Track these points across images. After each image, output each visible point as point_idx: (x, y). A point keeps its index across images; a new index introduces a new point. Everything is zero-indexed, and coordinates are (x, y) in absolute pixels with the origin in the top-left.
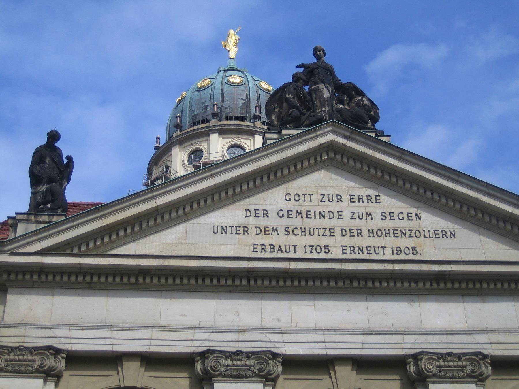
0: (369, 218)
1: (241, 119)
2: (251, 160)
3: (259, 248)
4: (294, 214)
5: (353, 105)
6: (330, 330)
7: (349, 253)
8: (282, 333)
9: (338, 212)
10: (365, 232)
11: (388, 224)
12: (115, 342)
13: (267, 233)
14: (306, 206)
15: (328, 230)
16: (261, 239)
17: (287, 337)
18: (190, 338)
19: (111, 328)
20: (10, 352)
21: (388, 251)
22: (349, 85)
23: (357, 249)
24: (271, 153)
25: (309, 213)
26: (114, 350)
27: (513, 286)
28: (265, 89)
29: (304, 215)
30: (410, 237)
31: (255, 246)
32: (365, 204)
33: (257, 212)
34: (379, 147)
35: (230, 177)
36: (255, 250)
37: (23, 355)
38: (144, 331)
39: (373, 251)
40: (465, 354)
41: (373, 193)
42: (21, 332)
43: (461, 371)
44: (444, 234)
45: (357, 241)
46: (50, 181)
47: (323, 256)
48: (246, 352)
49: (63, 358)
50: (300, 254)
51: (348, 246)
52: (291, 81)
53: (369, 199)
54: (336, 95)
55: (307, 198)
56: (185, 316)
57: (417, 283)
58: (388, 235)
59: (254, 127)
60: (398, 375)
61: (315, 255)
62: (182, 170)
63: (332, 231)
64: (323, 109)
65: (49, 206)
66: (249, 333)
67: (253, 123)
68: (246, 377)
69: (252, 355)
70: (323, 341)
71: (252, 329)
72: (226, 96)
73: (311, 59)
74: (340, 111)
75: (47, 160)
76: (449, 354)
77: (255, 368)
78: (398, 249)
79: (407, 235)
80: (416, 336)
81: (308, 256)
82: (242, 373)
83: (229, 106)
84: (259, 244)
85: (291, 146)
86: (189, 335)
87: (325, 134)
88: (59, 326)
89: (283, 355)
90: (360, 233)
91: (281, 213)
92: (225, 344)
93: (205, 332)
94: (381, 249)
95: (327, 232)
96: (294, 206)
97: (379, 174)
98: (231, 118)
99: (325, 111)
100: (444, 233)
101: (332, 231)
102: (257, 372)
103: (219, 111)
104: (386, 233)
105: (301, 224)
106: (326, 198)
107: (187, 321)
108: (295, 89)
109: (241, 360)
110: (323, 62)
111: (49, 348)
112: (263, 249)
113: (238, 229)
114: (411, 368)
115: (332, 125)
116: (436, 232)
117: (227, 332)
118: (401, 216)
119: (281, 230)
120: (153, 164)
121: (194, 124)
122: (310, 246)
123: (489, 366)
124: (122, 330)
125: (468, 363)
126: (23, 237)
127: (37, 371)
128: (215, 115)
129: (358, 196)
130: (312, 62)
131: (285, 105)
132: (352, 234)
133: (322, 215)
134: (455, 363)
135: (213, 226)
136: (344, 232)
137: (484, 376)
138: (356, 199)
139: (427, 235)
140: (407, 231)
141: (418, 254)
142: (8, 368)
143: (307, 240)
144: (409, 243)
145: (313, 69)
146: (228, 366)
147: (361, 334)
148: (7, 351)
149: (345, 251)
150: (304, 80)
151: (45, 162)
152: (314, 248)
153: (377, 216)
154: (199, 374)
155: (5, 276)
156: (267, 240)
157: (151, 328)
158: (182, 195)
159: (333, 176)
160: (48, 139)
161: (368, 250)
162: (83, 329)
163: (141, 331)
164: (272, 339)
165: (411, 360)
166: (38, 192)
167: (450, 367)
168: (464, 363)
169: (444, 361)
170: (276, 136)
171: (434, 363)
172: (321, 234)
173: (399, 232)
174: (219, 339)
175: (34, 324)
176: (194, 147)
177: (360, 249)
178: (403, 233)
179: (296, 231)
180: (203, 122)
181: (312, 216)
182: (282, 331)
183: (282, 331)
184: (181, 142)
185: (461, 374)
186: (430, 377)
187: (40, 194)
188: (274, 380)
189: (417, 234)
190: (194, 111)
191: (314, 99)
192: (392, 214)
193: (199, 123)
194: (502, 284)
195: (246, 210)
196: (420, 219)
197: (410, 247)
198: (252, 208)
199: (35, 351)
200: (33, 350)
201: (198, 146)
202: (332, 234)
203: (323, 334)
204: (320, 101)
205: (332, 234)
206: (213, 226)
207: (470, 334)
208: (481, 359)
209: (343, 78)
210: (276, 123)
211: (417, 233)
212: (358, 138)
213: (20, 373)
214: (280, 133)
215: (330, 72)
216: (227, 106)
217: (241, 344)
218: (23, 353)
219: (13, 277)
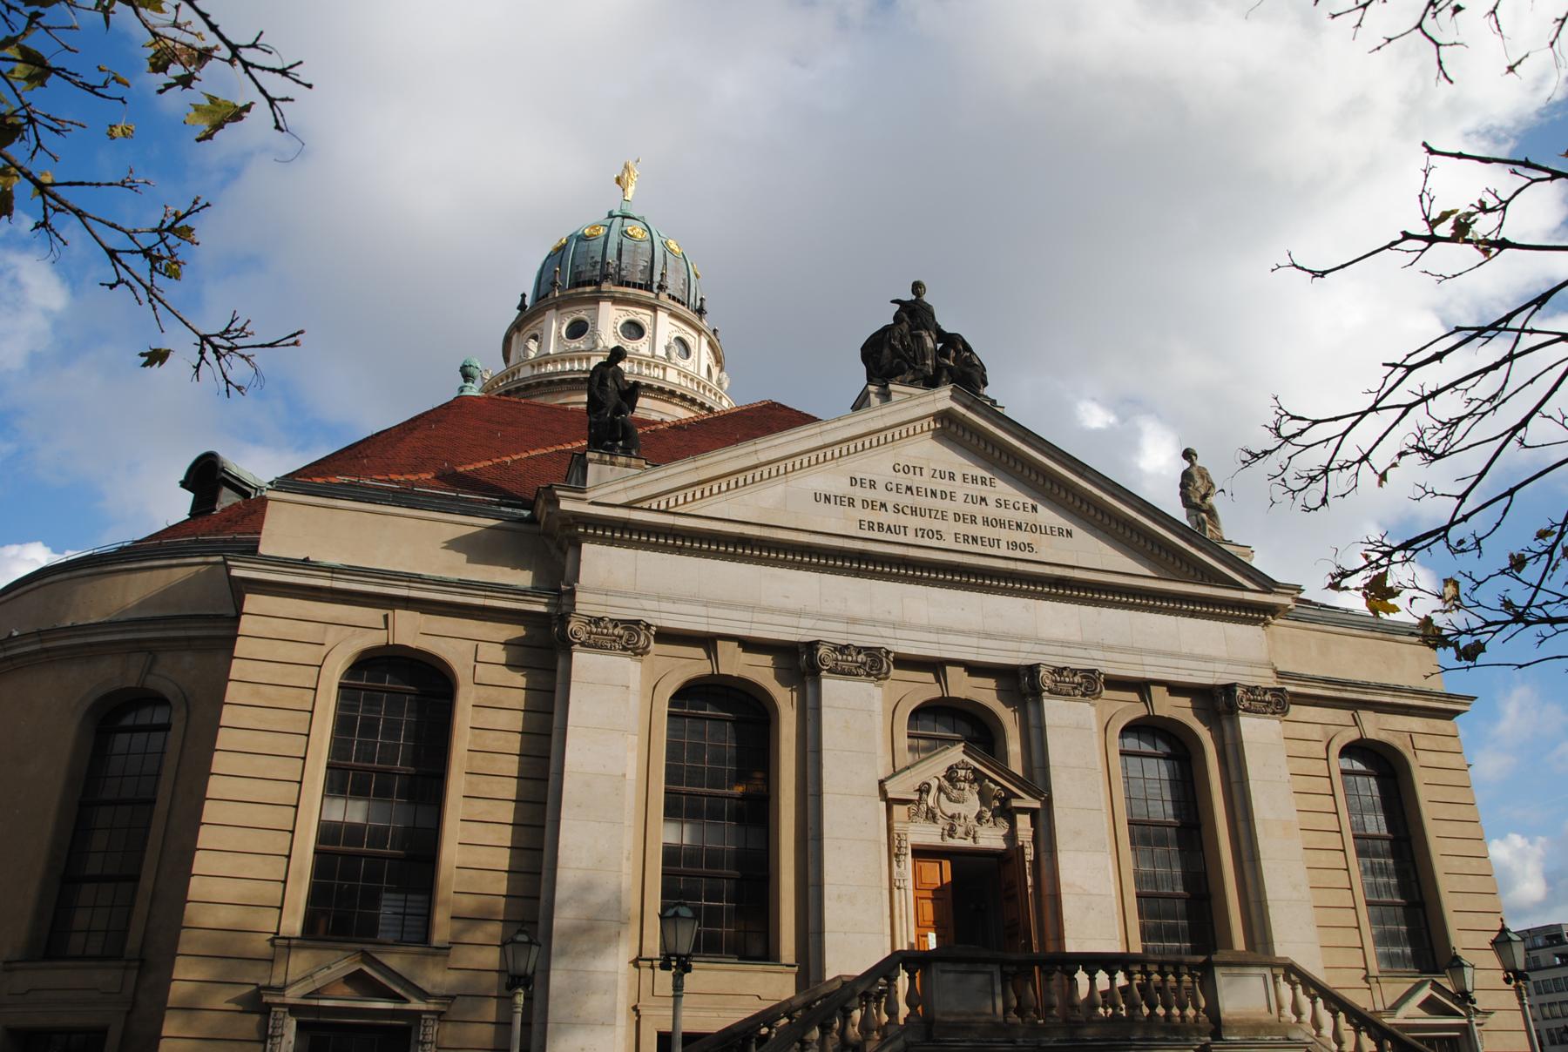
0: (983, 503)
10: (979, 520)
12: (711, 621)
14: (915, 480)
15: (940, 513)
17: (899, 633)
19: (706, 604)
30: (1025, 530)
41: (988, 475)
44: (1061, 533)
45: (972, 530)
53: (984, 482)
56: (787, 597)
60: (993, 678)
65: (621, 443)
70: (936, 641)
71: (863, 620)
73: (908, 296)
79: (1023, 528)
80: (813, 621)
86: (794, 621)
88: (646, 596)
92: (832, 635)
93: (811, 619)
95: (939, 515)
96: (904, 479)
97: (997, 454)
106: (937, 474)
112: (871, 528)
119: (890, 507)
120: (515, 329)
121: (578, 285)
122: (920, 529)
129: (972, 476)
130: (909, 299)
135: (816, 494)
136: (957, 517)
139: (1043, 531)
144: (1021, 537)
157: (752, 608)
159: (946, 449)
172: (933, 516)
176: (575, 316)
177: (975, 540)
178: (1019, 526)
182: (894, 626)
183: (894, 626)
184: (559, 305)
189: (1034, 528)
190: (578, 266)
206: (816, 494)
209: (948, 328)
213: (587, 647)
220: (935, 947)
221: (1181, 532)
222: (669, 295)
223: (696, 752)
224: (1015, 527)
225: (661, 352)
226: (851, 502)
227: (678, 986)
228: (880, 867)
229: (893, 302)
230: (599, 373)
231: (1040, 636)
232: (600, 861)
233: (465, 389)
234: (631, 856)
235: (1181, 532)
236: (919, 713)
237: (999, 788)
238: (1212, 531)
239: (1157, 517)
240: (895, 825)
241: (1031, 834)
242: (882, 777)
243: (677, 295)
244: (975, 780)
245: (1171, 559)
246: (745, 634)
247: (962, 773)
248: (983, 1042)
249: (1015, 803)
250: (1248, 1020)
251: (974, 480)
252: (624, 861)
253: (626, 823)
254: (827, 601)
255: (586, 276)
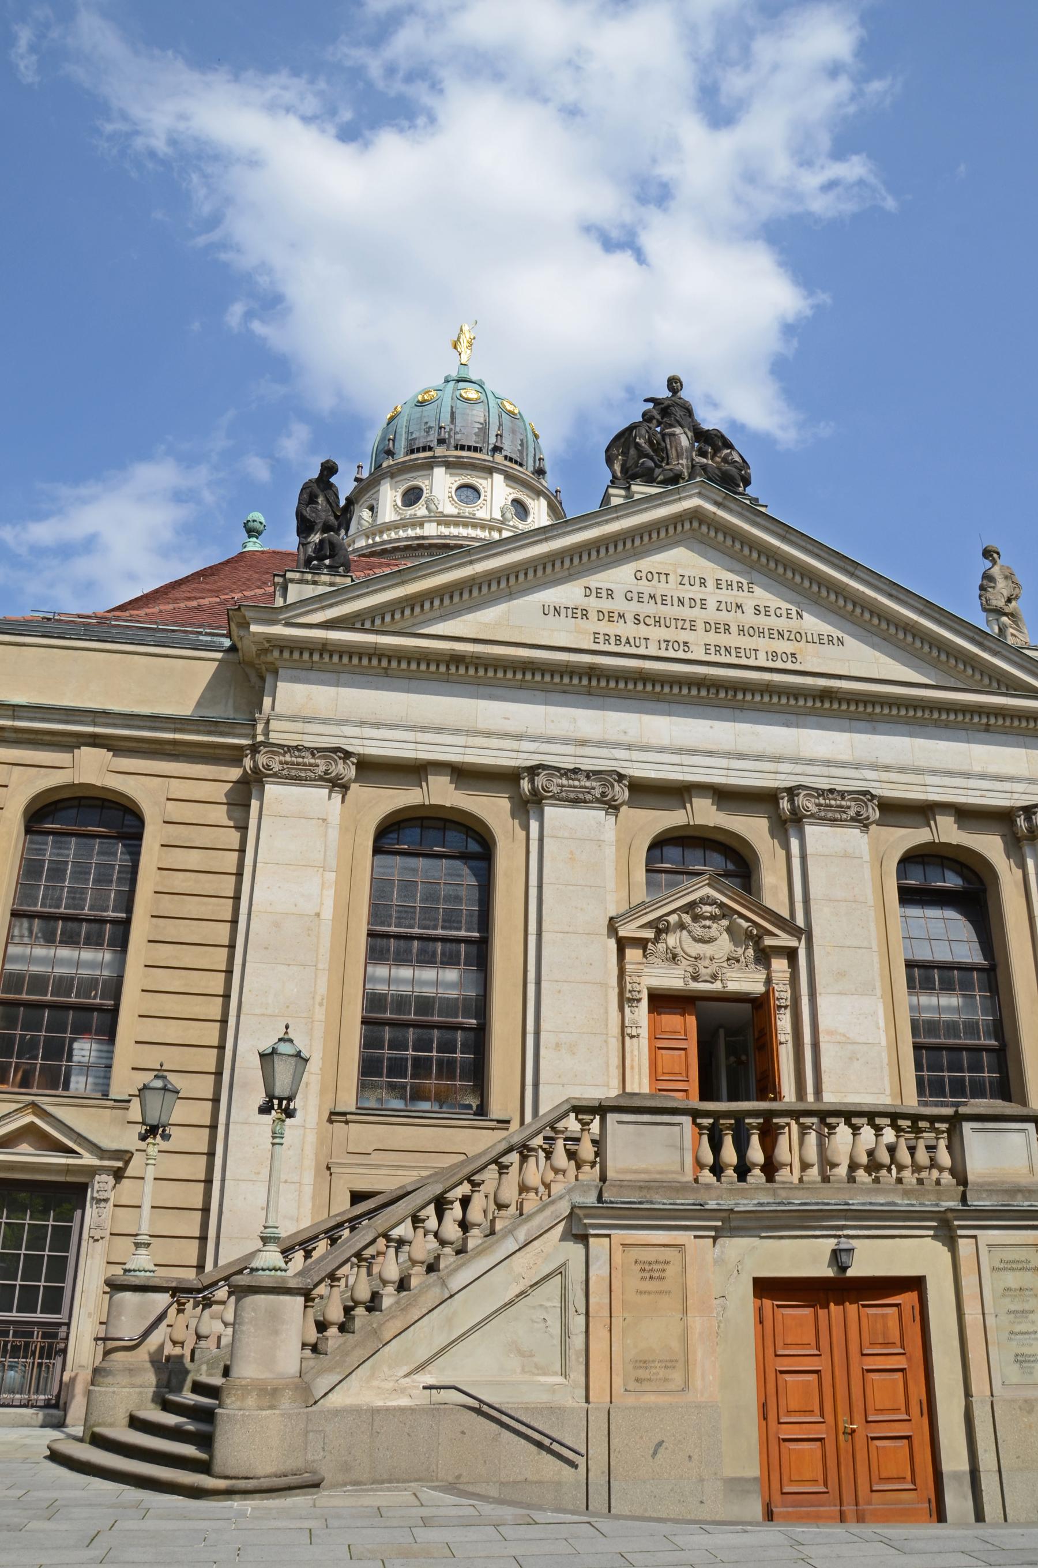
0: (739, 611)
1: (476, 449)
2: (596, 523)
3: (601, 637)
4: (646, 597)
5: (718, 459)
6: (689, 750)
7: (713, 654)
8: (630, 750)
9: (701, 600)
10: (734, 629)
11: (762, 621)
12: (420, 747)
13: (611, 619)
14: (660, 588)
15: (688, 622)
16: (604, 627)
17: (635, 755)
18: (515, 748)
19: (414, 728)
20: (285, 753)
21: (762, 655)
22: (715, 432)
23: (723, 649)
24: (622, 516)
25: (664, 598)
26: (418, 757)
27: (1032, 725)
28: (509, 411)
29: (659, 600)
31: (597, 636)
32: (735, 592)
33: (599, 591)
34: (758, 520)
35: (569, 543)
36: (597, 640)
37: (303, 757)
38: (457, 735)
39: (743, 654)
40: (850, 793)
42: (299, 726)
43: (844, 812)
45: (723, 640)
46: (327, 528)
47: (681, 655)
48: (585, 771)
49: (353, 764)
50: (652, 651)
51: (713, 645)
52: (641, 420)
54: (696, 444)
55: (663, 578)
56: (508, 719)
57: (796, 699)
58: (761, 635)
59: (493, 462)
61: (671, 654)
62: (393, 513)
63: (693, 623)
64: (681, 462)
65: (327, 562)
66: (589, 746)
67: (493, 456)
68: (585, 802)
69: (593, 775)
70: (679, 763)
71: (594, 742)
72: (458, 416)
73: (664, 393)
74: (704, 467)
75: (320, 500)
76: (831, 791)
77: (597, 790)
78: (774, 654)
79: (786, 637)
81: (663, 653)
82: (581, 796)
83: (461, 430)
84: (602, 633)
85: (647, 508)
86: (514, 744)
87: (690, 497)
89: (359, 755)
90: (727, 629)
91: (629, 595)
93: (534, 741)
94: (753, 652)
95: (687, 625)
97: (755, 555)
98: (462, 448)
99: (682, 465)
100: (830, 638)
101: (693, 623)
102: (599, 796)
103: (447, 436)
104: (760, 632)
105: (655, 612)
106: (686, 581)
107: (510, 727)
108: (647, 432)
109: (579, 780)
110: (680, 398)
111: (336, 750)
112: (607, 641)
113: (575, 611)
114: (785, 804)
115: (701, 486)
116: (821, 637)
117: (562, 744)
118: (778, 612)
119: (629, 617)
121: (412, 452)
122: (665, 641)
123: (876, 808)
124: (428, 732)
125: (853, 803)
126: (302, 602)
127: (321, 778)
128: (441, 442)
131: (632, 452)
132: (718, 630)
133: (681, 602)
134: (838, 802)
137: (870, 820)
138: (724, 586)
139: (810, 639)
140: (785, 631)
141: (798, 663)
142: (283, 772)
143: (662, 633)
144: (783, 646)
145: (669, 406)
146: (563, 786)
147: (726, 758)
148: (282, 751)
149: (597, 640)
150: (658, 421)
151: (318, 503)
152: (670, 644)
153: (749, 609)
154: (526, 794)
155: (276, 653)
156: (613, 629)
158: (508, 562)
160: (322, 471)
161: (737, 652)
162: (378, 728)
163: (453, 734)
164: (618, 756)
165: (785, 794)
166: (309, 543)
167: (831, 806)
168: (849, 803)
169: (824, 799)
170: (622, 492)
171: (813, 800)
172: (679, 627)
173: (776, 633)
174: (551, 751)
175: (315, 718)
178: (781, 635)
179: (647, 620)
180: (424, 449)
181: (669, 602)
182: (629, 747)
183: (629, 747)
184: (393, 473)
185: (844, 816)
186: (547, 798)
187: (311, 545)
188: (345, 788)
189: (798, 636)
190: (412, 433)
191: (669, 447)
192: (767, 609)
193: (418, 450)
194: (899, 709)
195: (585, 588)
196: (801, 617)
197: (788, 653)
198: (593, 585)
199: (318, 752)
200: (315, 752)
201: (415, 483)
202: (693, 628)
203: (681, 754)
204: (677, 450)
205: (693, 629)
207: (857, 768)
208: (868, 800)
210: (619, 474)
211: (798, 636)
212: (732, 506)
214: (628, 489)
215: (689, 411)
216: (458, 429)
217: (578, 760)
218: (303, 754)
219: (286, 654)
220: (920, 1125)
221: (971, 634)
222: (506, 457)
223: (407, 887)
224: (776, 635)
225: (497, 515)
226: (585, 614)
227: (277, 1136)
228: (606, 1012)
229: (646, 400)
230: (308, 491)
231: (802, 755)
232: (288, 1007)
233: (248, 544)
234: (325, 1001)
235: (971, 634)
236: (659, 844)
237: (750, 924)
238: (1016, 636)
239: (942, 619)
240: (627, 966)
241: (788, 975)
242: (613, 914)
243: (514, 456)
244: (724, 916)
245: (961, 666)
246: (458, 760)
247: (707, 908)
248: (664, 1204)
249: (768, 941)
250: (1003, 1183)
251: (729, 585)
252: (317, 1006)
253: (320, 966)
254: (553, 721)
255: (420, 443)
